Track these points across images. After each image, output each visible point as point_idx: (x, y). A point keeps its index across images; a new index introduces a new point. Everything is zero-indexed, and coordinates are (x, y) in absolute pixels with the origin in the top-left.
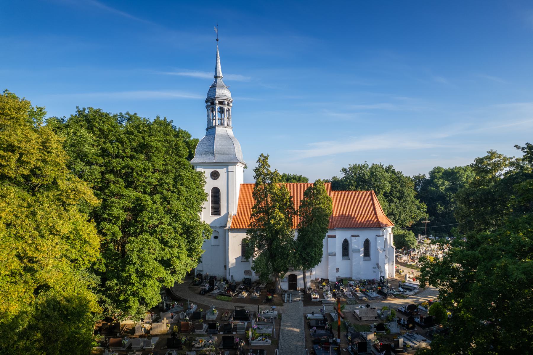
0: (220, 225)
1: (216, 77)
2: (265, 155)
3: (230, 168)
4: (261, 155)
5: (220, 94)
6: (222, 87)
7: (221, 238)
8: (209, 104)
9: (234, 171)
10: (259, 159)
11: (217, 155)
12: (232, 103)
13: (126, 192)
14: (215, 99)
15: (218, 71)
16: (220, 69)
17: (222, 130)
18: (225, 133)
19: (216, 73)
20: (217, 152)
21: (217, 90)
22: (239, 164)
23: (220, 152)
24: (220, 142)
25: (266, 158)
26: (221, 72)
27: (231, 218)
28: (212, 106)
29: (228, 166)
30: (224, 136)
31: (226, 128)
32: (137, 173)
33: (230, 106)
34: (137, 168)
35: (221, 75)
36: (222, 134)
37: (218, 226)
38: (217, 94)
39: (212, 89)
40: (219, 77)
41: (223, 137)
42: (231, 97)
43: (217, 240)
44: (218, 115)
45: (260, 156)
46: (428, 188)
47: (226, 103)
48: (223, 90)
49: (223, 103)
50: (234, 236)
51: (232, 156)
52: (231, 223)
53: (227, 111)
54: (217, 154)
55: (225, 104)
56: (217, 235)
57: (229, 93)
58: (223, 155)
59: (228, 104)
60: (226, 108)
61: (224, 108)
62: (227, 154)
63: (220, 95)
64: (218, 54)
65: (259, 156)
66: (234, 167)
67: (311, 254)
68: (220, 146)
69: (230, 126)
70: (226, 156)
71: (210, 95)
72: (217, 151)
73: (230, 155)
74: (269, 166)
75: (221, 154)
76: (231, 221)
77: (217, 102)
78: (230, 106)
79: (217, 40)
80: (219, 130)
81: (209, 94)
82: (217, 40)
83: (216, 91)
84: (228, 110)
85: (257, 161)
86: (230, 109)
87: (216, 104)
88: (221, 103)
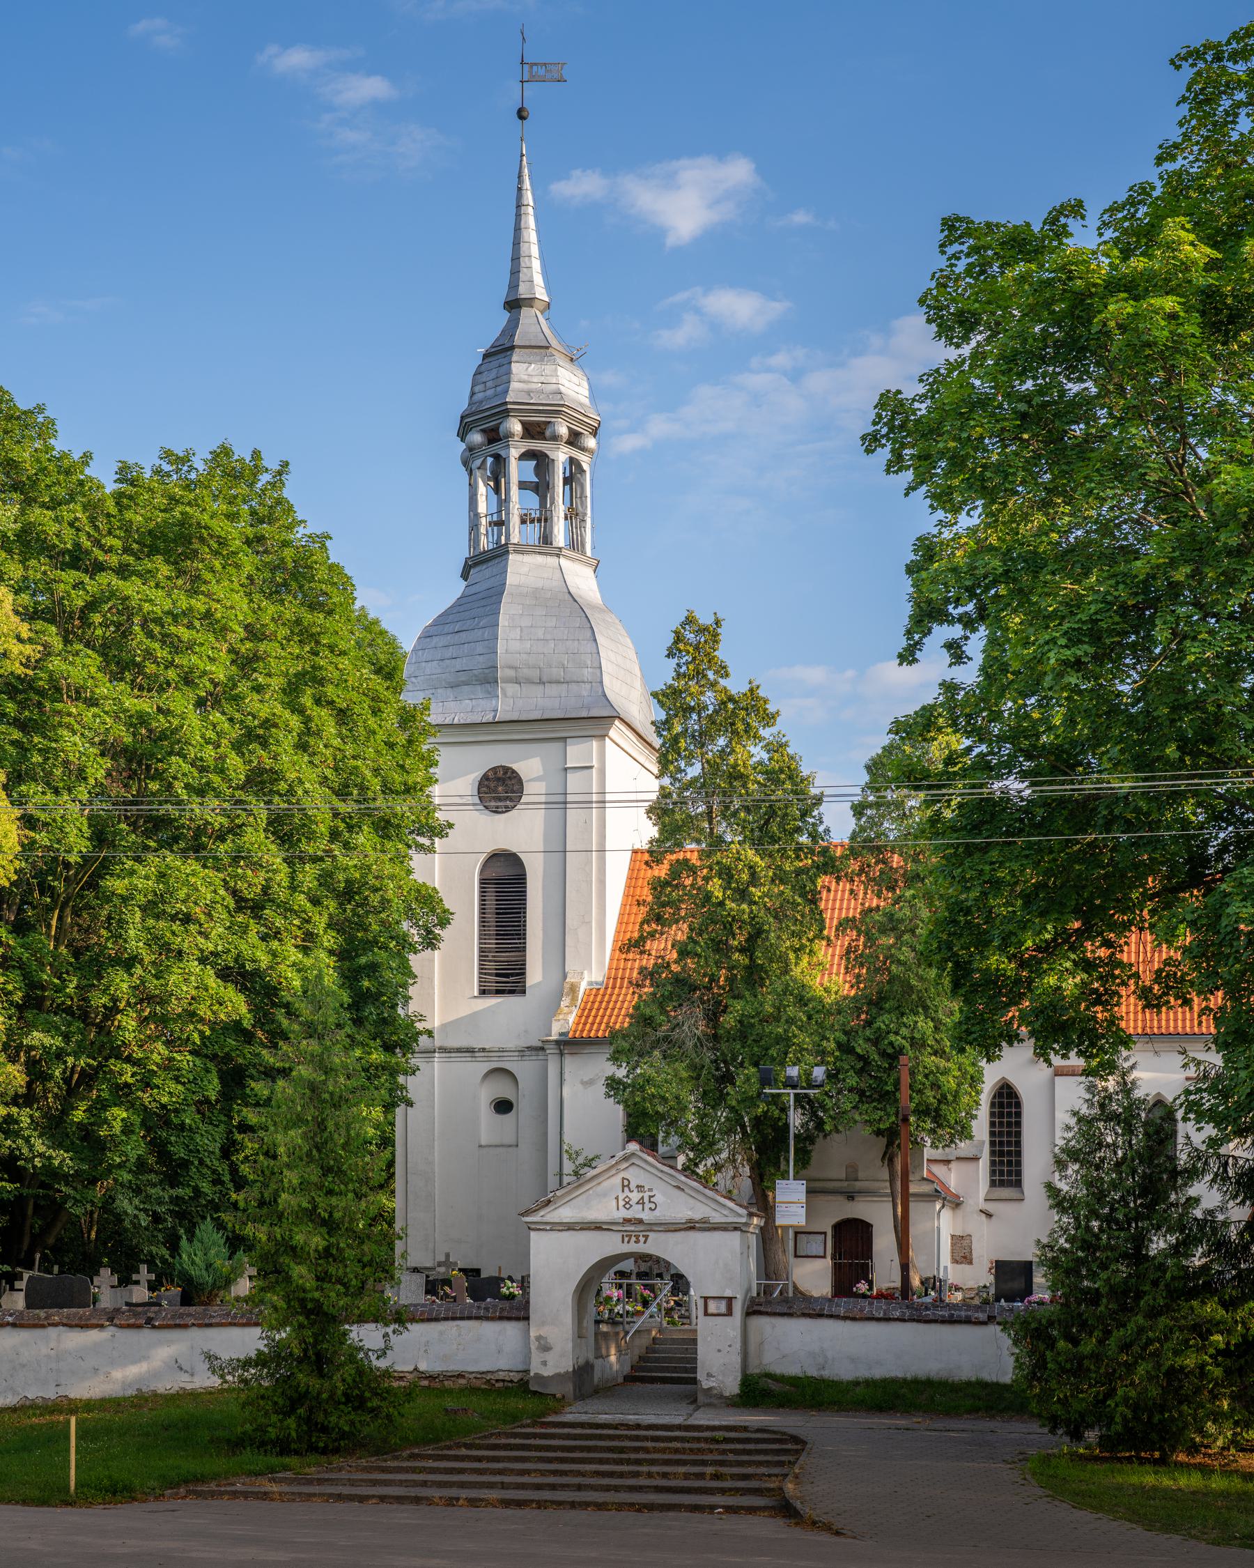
0: (523, 1043)
1: (514, 305)
2: (706, 619)
3: (576, 753)
4: (689, 621)
5: (534, 386)
6: (541, 349)
7: (525, 1107)
8: (476, 438)
9: (595, 763)
10: (678, 638)
11: (512, 689)
12: (595, 433)
13: (104, 689)
14: (504, 413)
15: (523, 270)
16: (536, 265)
17: (540, 566)
18: (556, 583)
19: (514, 285)
20: (511, 673)
21: (515, 367)
22: (617, 731)
23: (526, 672)
24: (526, 622)
25: (711, 634)
26: (538, 279)
27: (574, 999)
28: (495, 448)
29: (564, 739)
30: (549, 595)
31: (563, 561)
32: (143, 625)
33: (583, 449)
34: (147, 607)
35: (541, 294)
36: (540, 584)
37: (511, 1044)
38: (514, 385)
39: (495, 362)
40: (530, 302)
41: (540, 599)
42: (587, 401)
43: (508, 1118)
44: (519, 501)
45: (683, 625)
46: (1119, 694)
47: (563, 431)
48: (548, 369)
49: (548, 433)
50: (586, 1079)
51: (585, 690)
52: (572, 1019)
53: (568, 481)
54: (508, 680)
55: (555, 438)
56: (503, 1090)
57: (575, 379)
58: (541, 687)
59: (574, 439)
60: (561, 456)
61: (551, 455)
62: (558, 682)
63: (529, 393)
64: (527, 184)
65: (675, 625)
66: (595, 744)
67: (892, 1037)
68: (528, 645)
69: (583, 553)
70: (553, 690)
71: (479, 397)
72: (511, 667)
73: (574, 687)
74: (723, 671)
75: (530, 682)
76: (575, 1011)
77: (516, 427)
78: (583, 449)
79: (521, 115)
80: (525, 569)
81: (477, 389)
82: (521, 115)
83: (509, 373)
84: (574, 475)
85: (670, 649)
86: (585, 466)
87: (509, 435)
88: (533, 431)
